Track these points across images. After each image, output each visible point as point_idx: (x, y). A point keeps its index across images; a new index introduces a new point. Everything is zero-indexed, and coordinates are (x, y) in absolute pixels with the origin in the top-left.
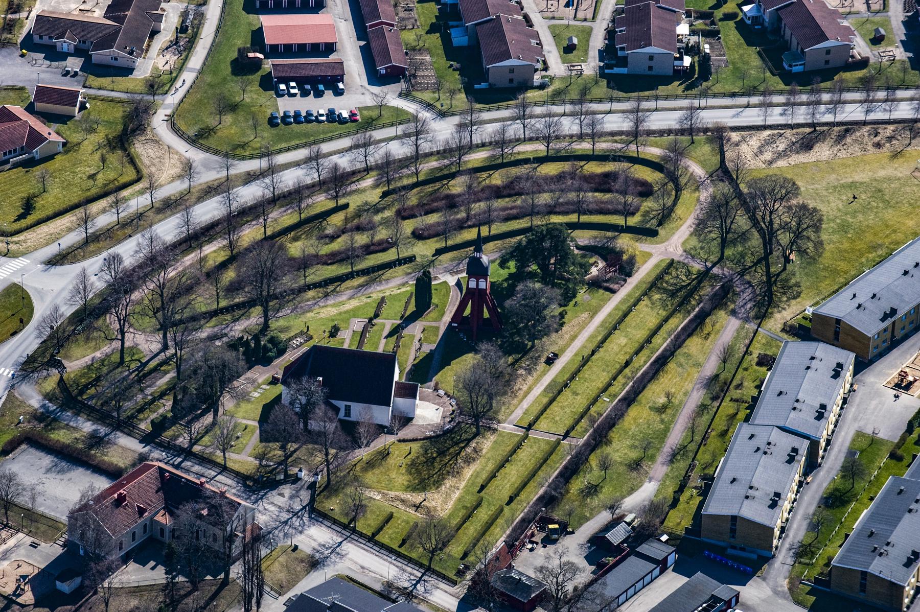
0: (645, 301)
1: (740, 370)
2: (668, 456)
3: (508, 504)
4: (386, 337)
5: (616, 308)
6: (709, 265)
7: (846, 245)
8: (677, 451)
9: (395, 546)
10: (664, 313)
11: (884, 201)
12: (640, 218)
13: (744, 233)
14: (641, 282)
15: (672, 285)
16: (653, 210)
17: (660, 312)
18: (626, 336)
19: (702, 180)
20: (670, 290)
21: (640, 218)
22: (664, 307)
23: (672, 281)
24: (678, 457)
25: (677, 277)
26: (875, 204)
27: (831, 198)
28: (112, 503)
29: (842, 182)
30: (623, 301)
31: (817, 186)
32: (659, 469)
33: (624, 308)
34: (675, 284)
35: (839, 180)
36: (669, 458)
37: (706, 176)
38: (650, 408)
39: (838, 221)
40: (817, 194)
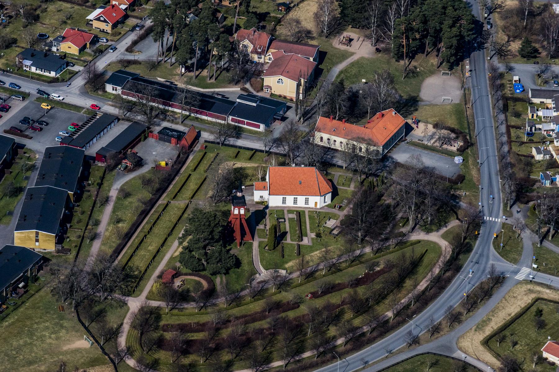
0: (143, 269)
1: (79, 246)
2: (110, 200)
3: (190, 175)
4: (287, 233)
5: (159, 263)
6: (109, 297)
7: (28, 323)
8: (106, 203)
9: (241, 151)
10: (130, 264)
11: (7, 355)
12: (160, 324)
13: (93, 321)
14: (149, 279)
15: (129, 281)
16: (153, 330)
17: (132, 265)
18: (149, 251)
19: (126, 356)
20: (130, 278)
21: (160, 324)
22: (131, 268)
23: (130, 283)
24: (104, 200)
25: (127, 286)
26: (14, 352)
27: (42, 353)
28: (442, 331)
29: (36, 365)
30: (156, 267)
31: (52, 361)
32: (114, 193)
33: (154, 264)
34: (127, 282)
35: (38, 366)
36: (109, 199)
37: (124, 359)
38: (126, 221)
39: (35, 338)
40: (51, 355)
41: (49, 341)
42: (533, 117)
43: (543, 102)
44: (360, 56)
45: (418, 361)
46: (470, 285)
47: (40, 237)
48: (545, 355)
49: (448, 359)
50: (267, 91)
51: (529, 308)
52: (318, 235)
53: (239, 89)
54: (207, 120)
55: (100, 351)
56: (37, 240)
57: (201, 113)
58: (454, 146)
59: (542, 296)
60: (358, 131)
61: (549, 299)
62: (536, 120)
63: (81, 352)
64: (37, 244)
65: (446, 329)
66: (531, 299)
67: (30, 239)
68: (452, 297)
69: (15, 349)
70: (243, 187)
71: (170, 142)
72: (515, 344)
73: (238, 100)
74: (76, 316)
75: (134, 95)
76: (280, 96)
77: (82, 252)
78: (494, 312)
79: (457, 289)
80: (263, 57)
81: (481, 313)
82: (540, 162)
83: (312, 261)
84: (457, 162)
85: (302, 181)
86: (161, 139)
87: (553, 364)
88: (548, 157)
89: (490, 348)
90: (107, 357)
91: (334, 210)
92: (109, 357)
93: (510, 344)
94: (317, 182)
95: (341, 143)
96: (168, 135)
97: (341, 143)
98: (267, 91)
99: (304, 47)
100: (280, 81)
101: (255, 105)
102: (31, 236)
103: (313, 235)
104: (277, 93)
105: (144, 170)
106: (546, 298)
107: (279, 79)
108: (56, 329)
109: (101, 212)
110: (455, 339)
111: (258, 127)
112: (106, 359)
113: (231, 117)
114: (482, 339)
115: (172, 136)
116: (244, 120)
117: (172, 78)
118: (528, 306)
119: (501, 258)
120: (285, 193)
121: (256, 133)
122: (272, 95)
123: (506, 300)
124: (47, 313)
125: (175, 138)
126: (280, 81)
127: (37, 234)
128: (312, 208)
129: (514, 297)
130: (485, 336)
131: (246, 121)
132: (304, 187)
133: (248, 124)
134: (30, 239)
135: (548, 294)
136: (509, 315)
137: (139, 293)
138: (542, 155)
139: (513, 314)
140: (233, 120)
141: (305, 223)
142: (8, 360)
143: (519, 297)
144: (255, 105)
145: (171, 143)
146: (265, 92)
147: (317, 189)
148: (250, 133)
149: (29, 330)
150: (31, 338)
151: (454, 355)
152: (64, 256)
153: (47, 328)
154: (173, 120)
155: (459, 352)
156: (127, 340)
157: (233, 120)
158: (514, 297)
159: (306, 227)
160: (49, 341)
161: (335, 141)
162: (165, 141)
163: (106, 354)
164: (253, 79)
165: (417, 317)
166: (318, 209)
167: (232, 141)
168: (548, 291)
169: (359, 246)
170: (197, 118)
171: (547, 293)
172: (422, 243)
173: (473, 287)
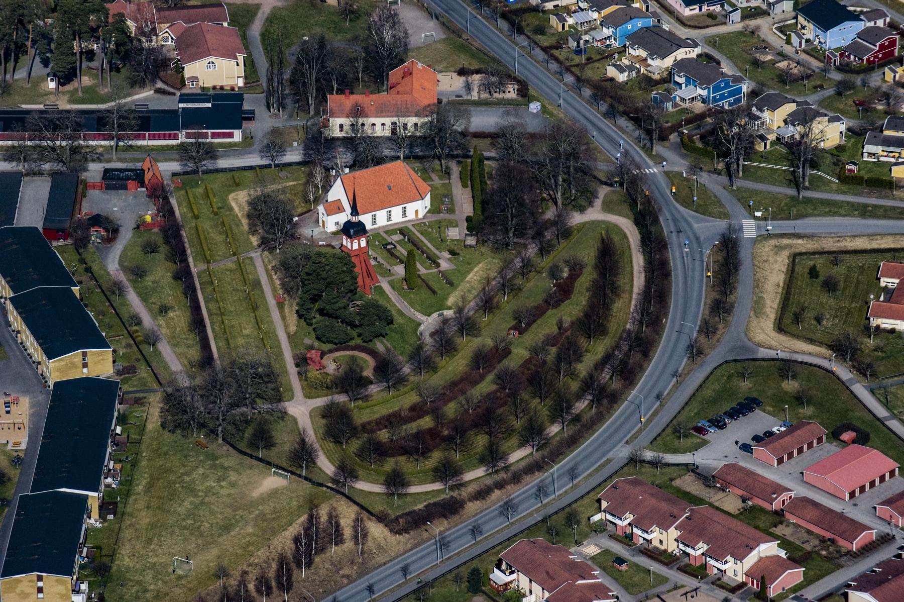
26: (190, 522)
27: (229, 510)
41: (223, 492)
42: (563, 28)
43: (557, 6)
44: (271, 6)
45: (723, 376)
46: (697, 263)
47: (89, 359)
48: (875, 322)
49: (758, 363)
50: (193, 85)
51: (793, 271)
52: (453, 253)
53: (152, 92)
54: (148, 146)
55: (308, 485)
56: (85, 365)
57: (137, 137)
58: (509, 92)
59: (797, 251)
60: (393, 102)
61: (810, 250)
62: (570, 31)
63: (282, 493)
64: (85, 370)
65: (657, 337)
66: (786, 258)
67: (74, 366)
68: (689, 282)
69: (187, 517)
70: (296, 219)
71: (125, 188)
72: (819, 320)
73: (181, 105)
74: (231, 449)
75: (11, 137)
76: (214, 88)
77: (155, 364)
78: (757, 285)
79: (685, 271)
80: (154, 38)
81: (742, 293)
82: (627, 83)
83: (473, 288)
84: (535, 111)
85: (391, 185)
86: (109, 188)
87: (893, 331)
88: (634, 74)
89: (785, 332)
90: (324, 488)
91: (441, 215)
92: (328, 487)
93: (814, 322)
94: (410, 181)
95: (383, 125)
96: (119, 178)
97: (383, 125)
98: (193, 85)
99: (185, 11)
100: (211, 65)
101: (209, 105)
102: (76, 360)
103: (446, 254)
104: (209, 84)
105: (126, 235)
106: (804, 251)
107: (209, 63)
108: (219, 474)
109: (125, 303)
110: (743, 335)
111: (231, 135)
112: (326, 492)
113: (184, 132)
114: (772, 326)
115: (128, 178)
116: (206, 131)
117: (46, 100)
118: (790, 268)
119: (703, 216)
120: (374, 208)
121: (230, 145)
122: (203, 89)
123: (759, 268)
124: (186, 456)
125: (132, 180)
126: (211, 65)
127: (84, 355)
128: (413, 220)
129: (765, 261)
130: (773, 320)
131: (210, 131)
132: (396, 192)
133: (214, 135)
134: (74, 366)
135: (802, 245)
136: (778, 285)
137: (290, 394)
138: (626, 74)
139: (781, 284)
140: (188, 136)
141: (422, 242)
142: (192, 534)
143: (771, 260)
144: (209, 105)
145: (127, 189)
146: (190, 88)
147: (415, 190)
148: (230, 147)
149: (183, 486)
150: (196, 496)
151: (760, 356)
152: (133, 377)
153: (205, 477)
154: (98, 158)
155: (761, 349)
156: (330, 461)
157: (188, 136)
158: (765, 261)
159: (427, 247)
160: (223, 492)
161: (374, 125)
162: (115, 188)
163: (321, 485)
164: (162, 74)
165: (669, 320)
166: (421, 219)
167: (208, 164)
168: (800, 241)
169: (514, 252)
170: (131, 146)
171: (801, 245)
172: (588, 226)
173: (703, 264)
